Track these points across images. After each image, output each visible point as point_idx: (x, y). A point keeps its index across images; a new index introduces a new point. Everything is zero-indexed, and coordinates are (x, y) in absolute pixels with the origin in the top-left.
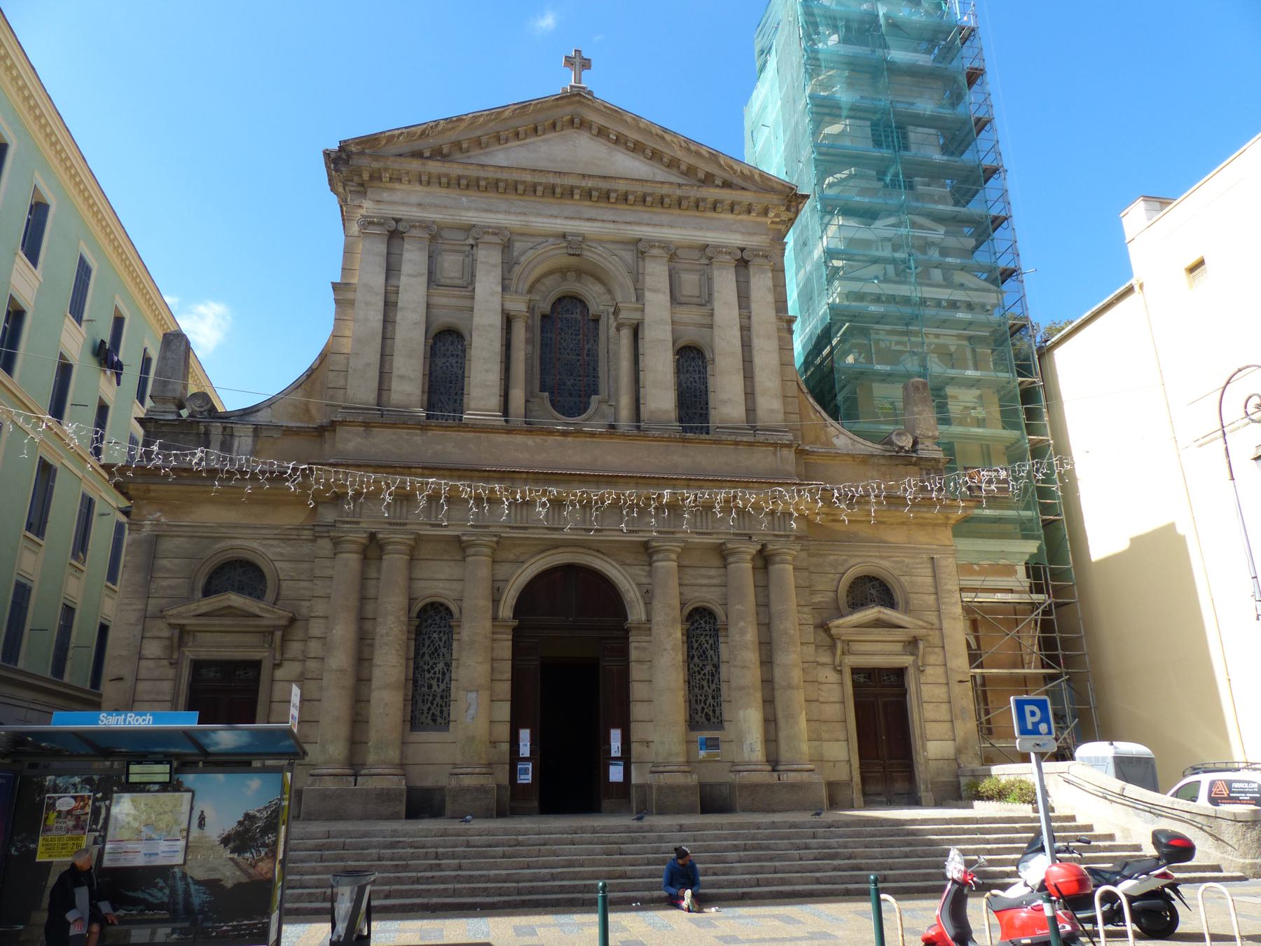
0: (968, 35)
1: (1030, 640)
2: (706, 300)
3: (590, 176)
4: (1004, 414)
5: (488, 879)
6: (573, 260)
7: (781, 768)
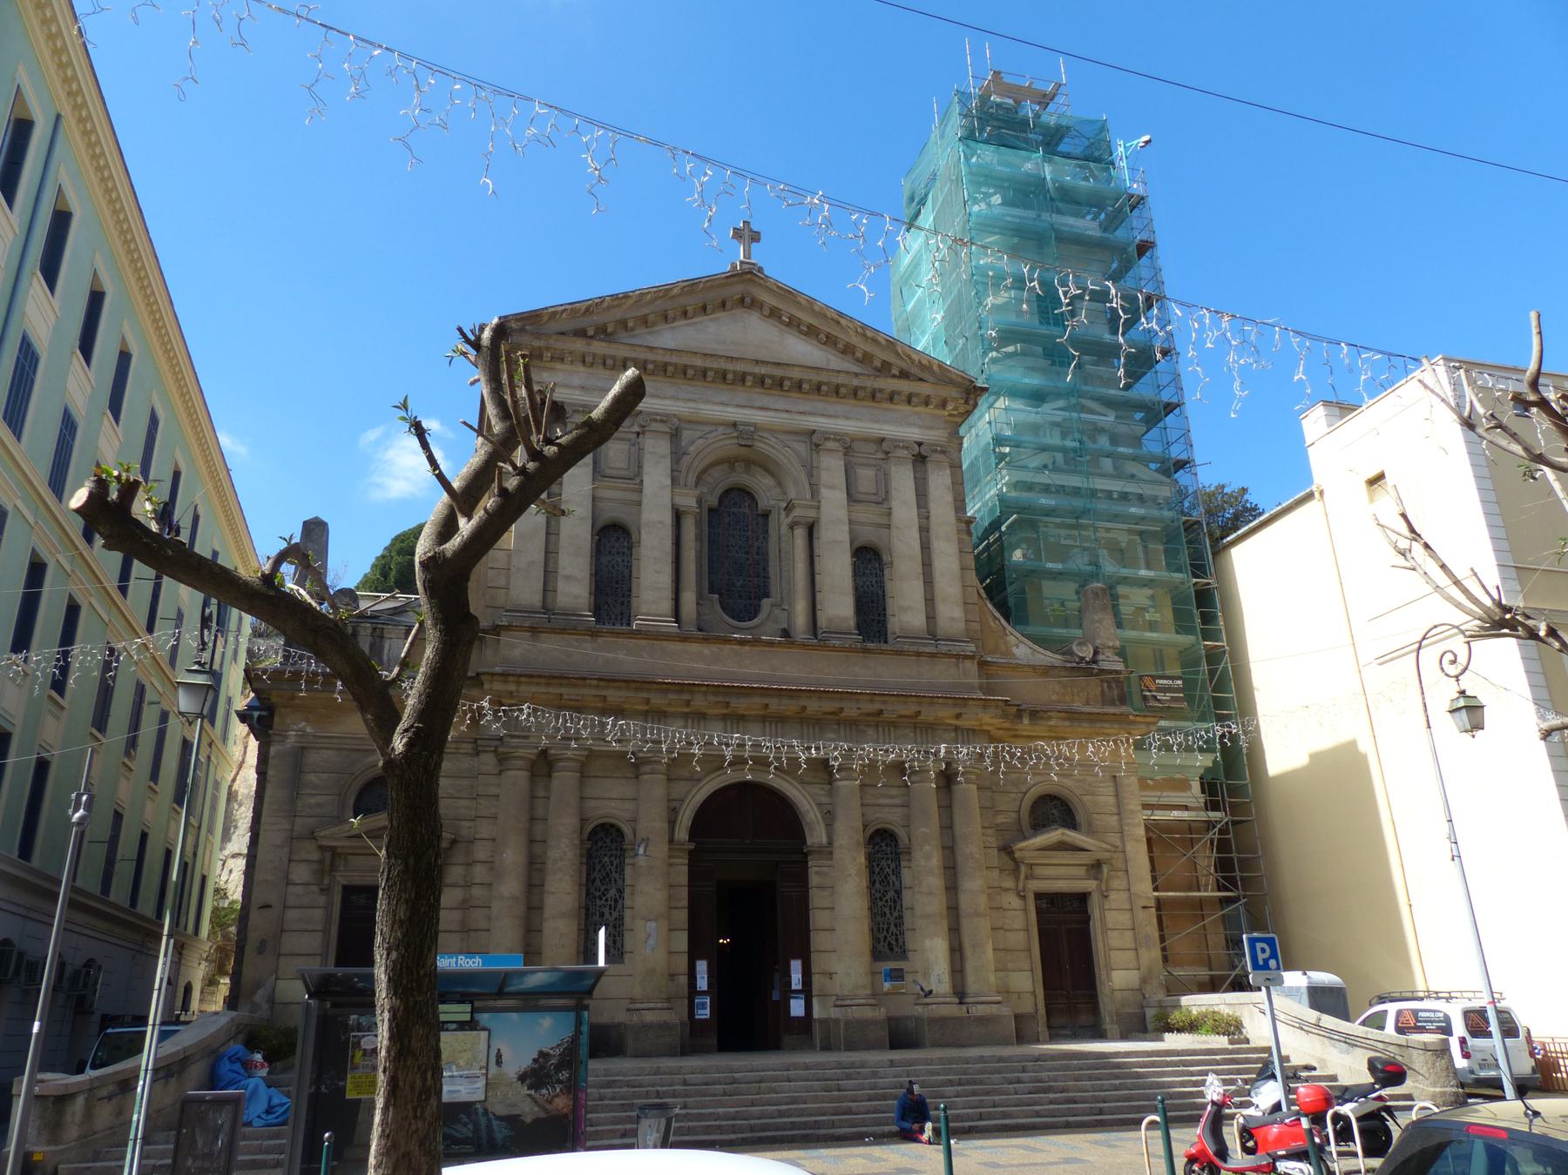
0: (1138, 202)
1: (1206, 860)
2: (882, 499)
3: (763, 362)
4: (1176, 612)
5: (718, 1117)
6: (744, 451)
7: (968, 1000)
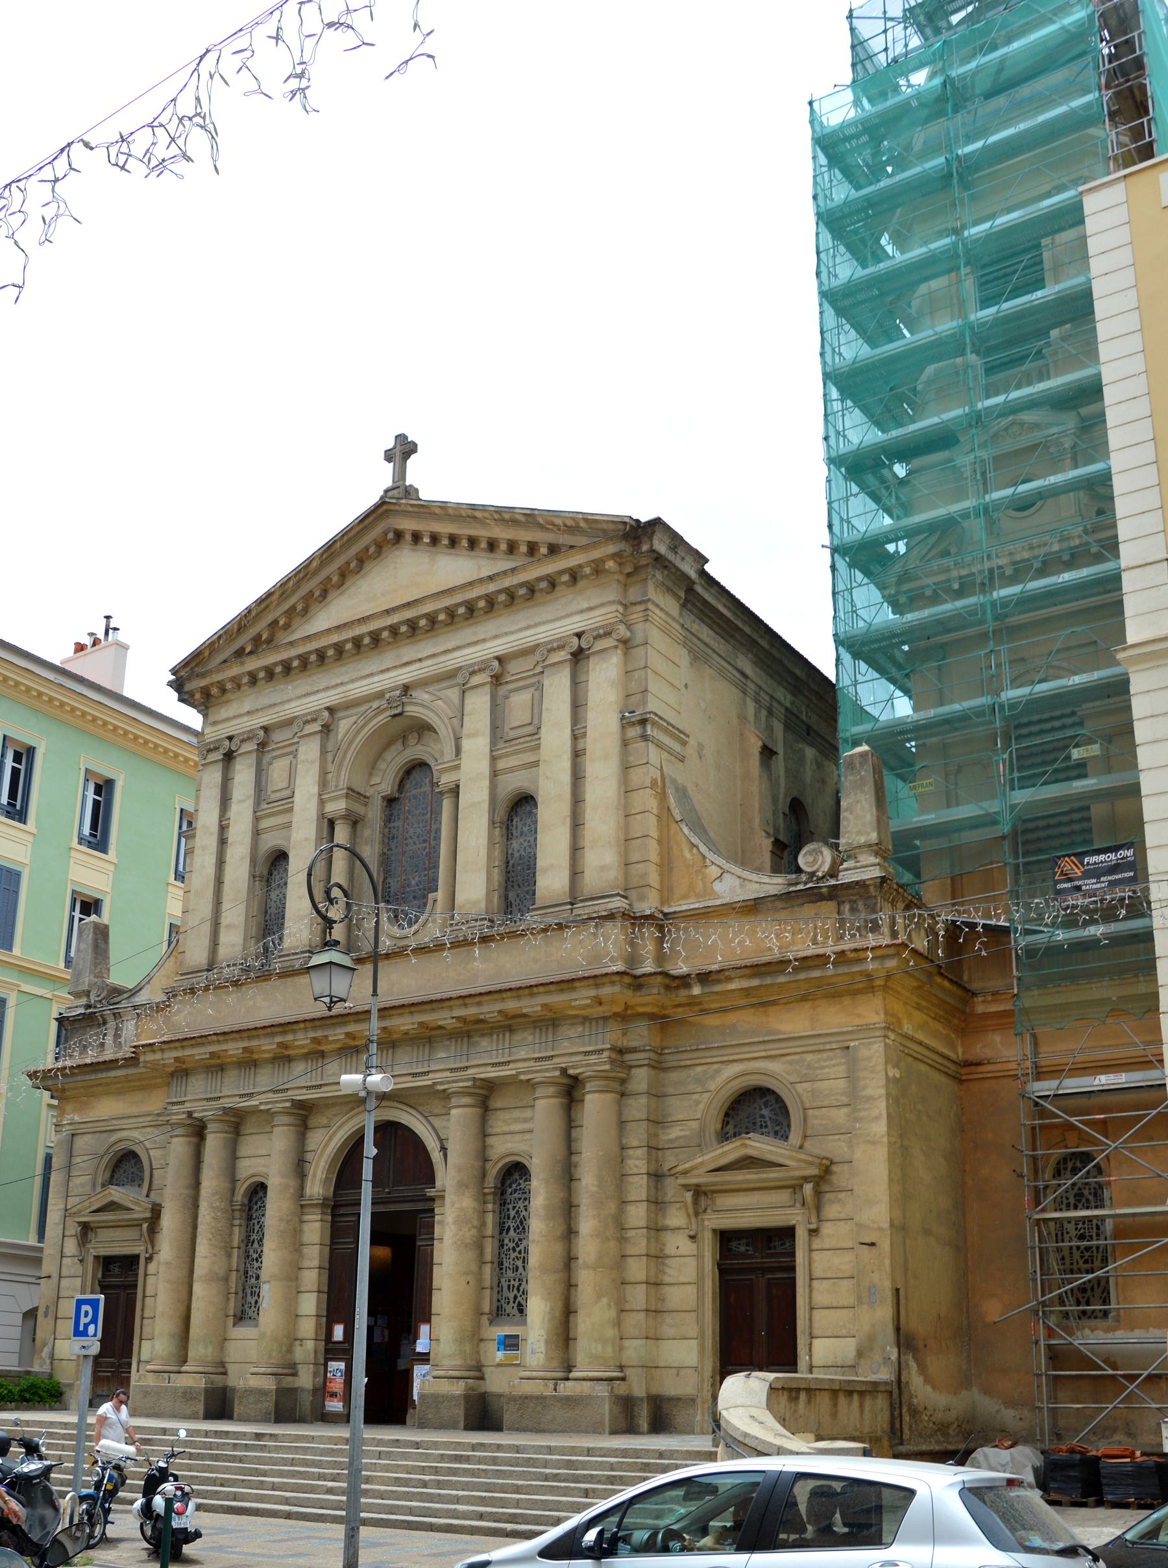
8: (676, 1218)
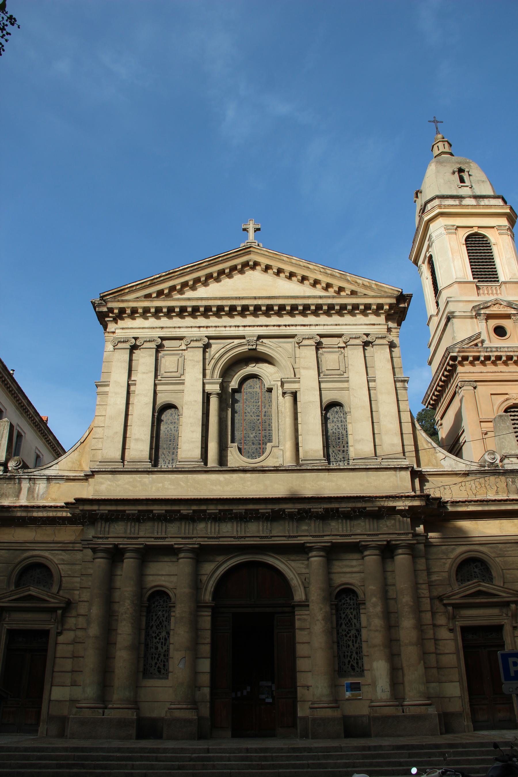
2: (342, 376)
8: (442, 620)
